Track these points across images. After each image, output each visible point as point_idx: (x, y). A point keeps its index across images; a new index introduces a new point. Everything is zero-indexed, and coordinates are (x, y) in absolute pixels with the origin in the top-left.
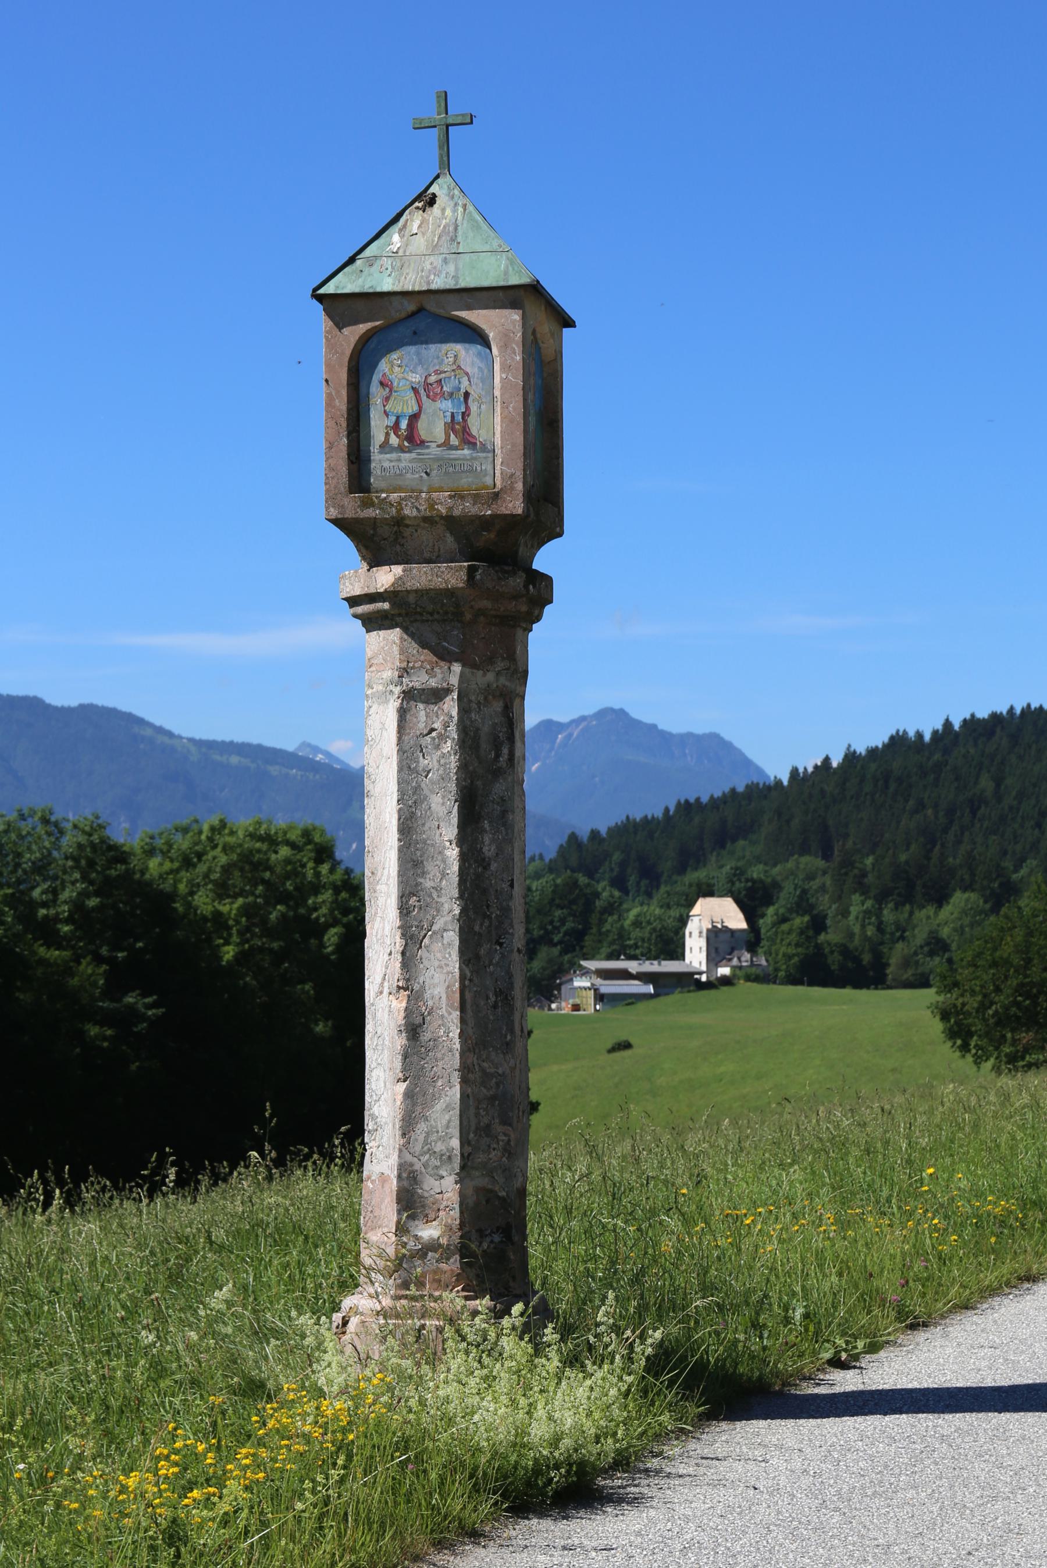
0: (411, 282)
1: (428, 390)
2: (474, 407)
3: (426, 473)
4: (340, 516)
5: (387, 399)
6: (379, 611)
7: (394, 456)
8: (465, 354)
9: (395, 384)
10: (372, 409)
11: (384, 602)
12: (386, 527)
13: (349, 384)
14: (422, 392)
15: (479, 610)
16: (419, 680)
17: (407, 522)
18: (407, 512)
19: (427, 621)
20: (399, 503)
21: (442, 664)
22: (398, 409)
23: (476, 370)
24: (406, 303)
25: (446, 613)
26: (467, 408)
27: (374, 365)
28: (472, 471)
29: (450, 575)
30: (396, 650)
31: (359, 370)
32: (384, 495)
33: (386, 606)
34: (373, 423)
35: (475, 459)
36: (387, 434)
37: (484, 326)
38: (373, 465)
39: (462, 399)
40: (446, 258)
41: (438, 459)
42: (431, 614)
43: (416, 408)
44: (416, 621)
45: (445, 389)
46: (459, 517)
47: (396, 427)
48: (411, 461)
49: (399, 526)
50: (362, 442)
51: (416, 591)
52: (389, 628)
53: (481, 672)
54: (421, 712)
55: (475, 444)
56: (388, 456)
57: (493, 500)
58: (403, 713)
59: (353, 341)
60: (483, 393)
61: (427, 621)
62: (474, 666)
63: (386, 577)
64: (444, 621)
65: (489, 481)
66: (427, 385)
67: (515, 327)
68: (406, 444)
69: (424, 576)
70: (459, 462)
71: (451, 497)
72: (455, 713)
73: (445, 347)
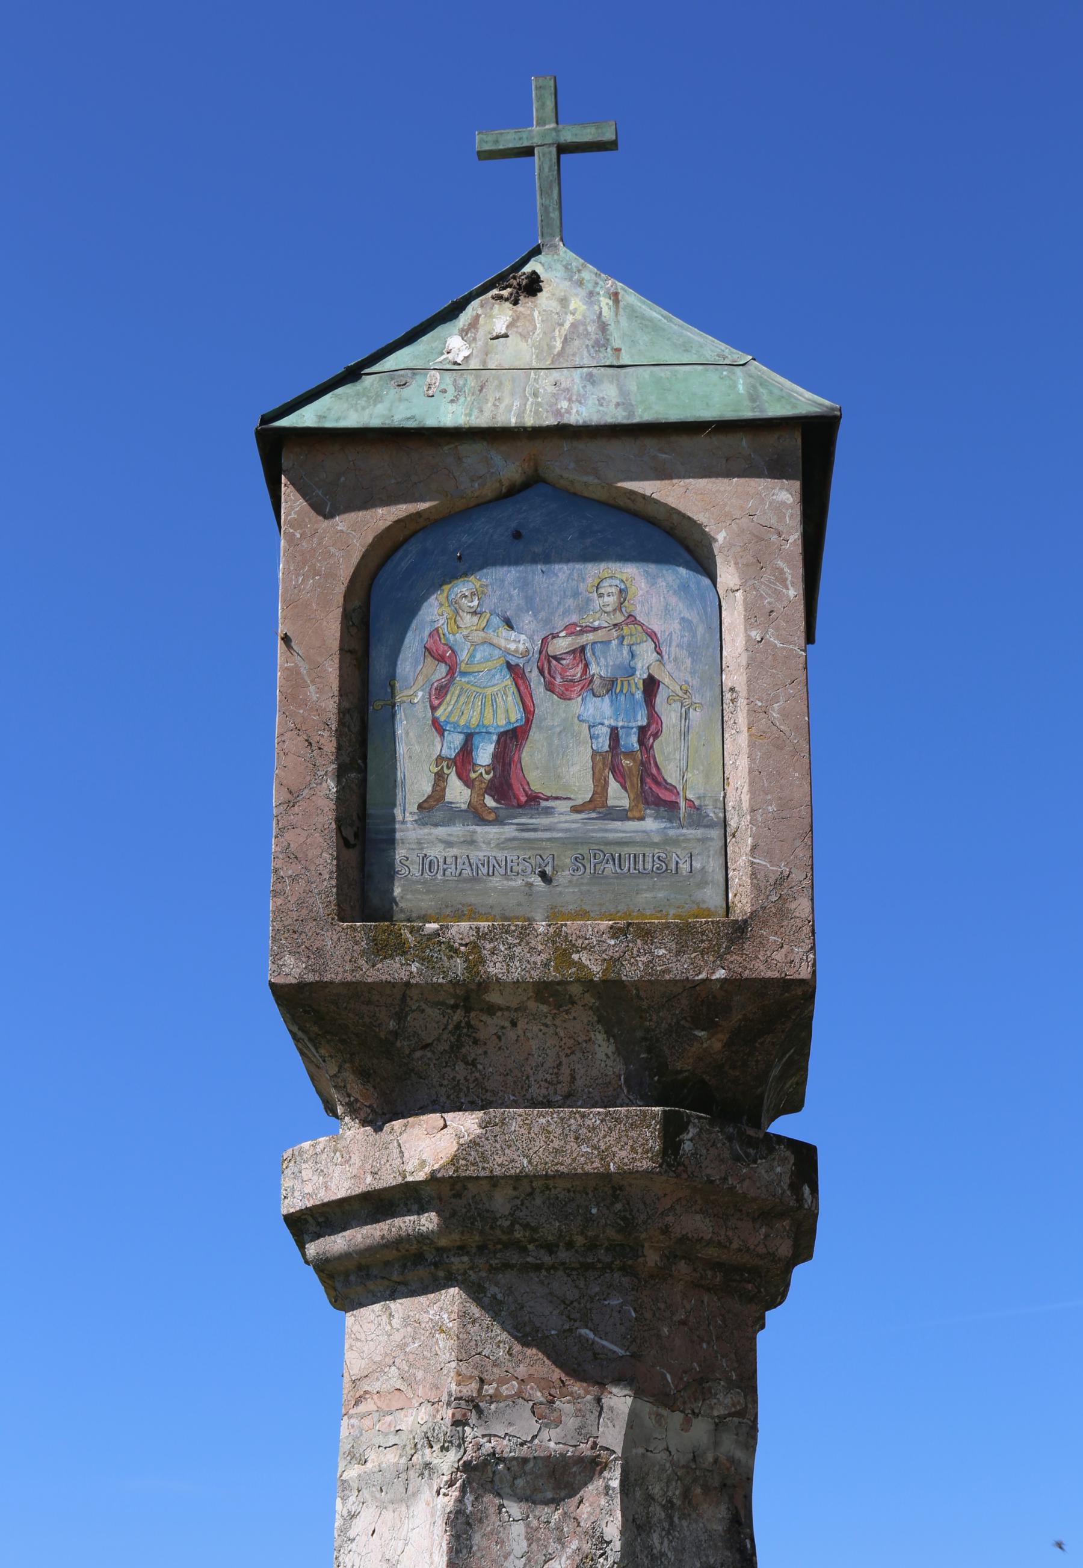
0: (509, 409)
1: (555, 671)
2: (669, 715)
3: (543, 875)
4: (310, 978)
5: (442, 691)
6: (398, 1242)
7: (457, 830)
8: (650, 589)
9: (463, 656)
10: (400, 715)
11: (421, 1211)
12: (433, 1013)
13: (344, 650)
14: (534, 676)
15: (683, 1239)
16: (514, 1432)
17: (494, 997)
18: (495, 968)
19: (538, 1268)
20: (475, 947)
21: (577, 1388)
22: (471, 717)
23: (676, 626)
24: (497, 459)
25: (592, 1246)
26: (653, 716)
27: (411, 610)
28: (664, 871)
29: (617, 1139)
30: (445, 1348)
31: (373, 614)
32: (433, 926)
33: (428, 1222)
34: (402, 749)
35: (675, 842)
36: (440, 778)
37: (700, 517)
38: (400, 853)
39: (639, 695)
40: (590, 375)
41: (573, 841)
42: (551, 1248)
43: (516, 716)
44: (507, 1266)
45: (594, 669)
46: (635, 984)
47: (464, 760)
48: (504, 844)
49: (468, 1009)
50: (374, 796)
51: (517, 1180)
52: (424, 1290)
53: (678, 1417)
54: (513, 1525)
55: (673, 806)
56: (441, 831)
57: (732, 942)
58: (462, 1528)
59: (359, 544)
60: (695, 682)
61: (538, 1268)
62: (664, 1399)
63: (427, 1144)
64: (586, 1267)
65: (712, 897)
66: (547, 661)
67: (781, 518)
68: (490, 802)
69: (538, 1140)
70: (632, 850)
71: (616, 932)
72: (613, 1529)
73: (594, 571)
